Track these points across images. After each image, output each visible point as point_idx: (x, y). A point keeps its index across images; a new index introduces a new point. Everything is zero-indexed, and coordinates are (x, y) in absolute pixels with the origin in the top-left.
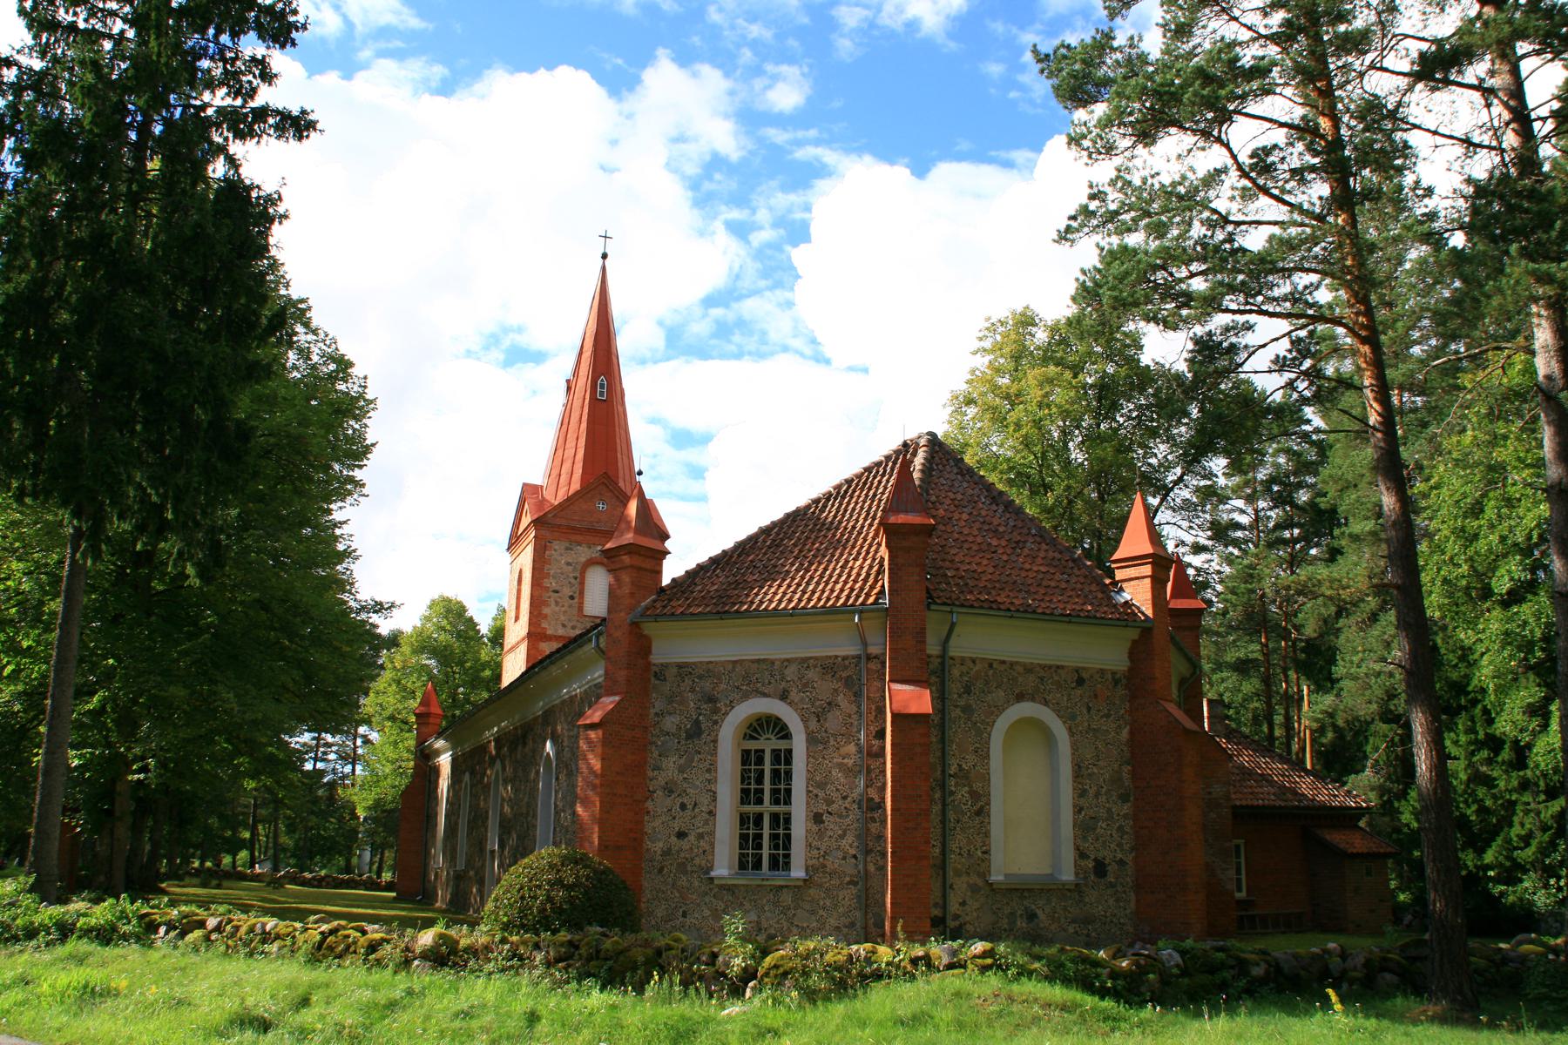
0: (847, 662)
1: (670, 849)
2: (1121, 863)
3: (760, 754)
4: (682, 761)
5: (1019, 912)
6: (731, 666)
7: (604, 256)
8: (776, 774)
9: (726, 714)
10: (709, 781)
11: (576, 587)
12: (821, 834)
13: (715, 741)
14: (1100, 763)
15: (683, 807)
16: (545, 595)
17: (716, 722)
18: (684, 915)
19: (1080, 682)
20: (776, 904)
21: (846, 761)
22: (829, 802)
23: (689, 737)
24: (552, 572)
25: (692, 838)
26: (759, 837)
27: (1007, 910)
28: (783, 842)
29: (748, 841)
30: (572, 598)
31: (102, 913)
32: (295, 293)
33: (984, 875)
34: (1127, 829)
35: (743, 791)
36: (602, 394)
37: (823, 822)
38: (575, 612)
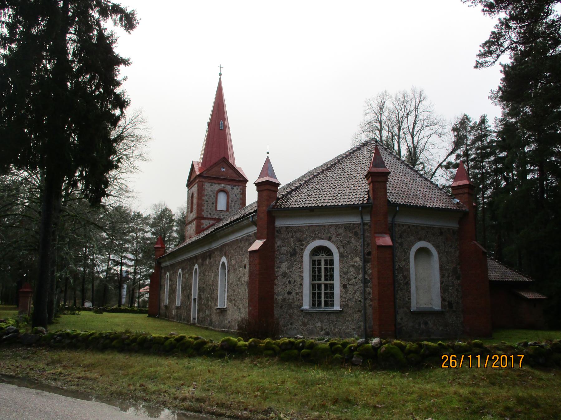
0: (355, 226)
1: (285, 299)
2: (458, 303)
3: (319, 262)
5: (422, 322)
7: (220, 75)
8: (326, 270)
9: (306, 246)
10: (300, 272)
11: (214, 200)
12: (346, 292)
13: (302, 257)
15: (290, 282)
17: (302, 249)
18: (291, 324)
19: (441, 233)
21: (355, 264)
25: (294, 294)
28: (330, 295)
33: (409, 308)
34: (460, 290)
35: (313, 276)
36: (221, 127)
37: (347, 288)
38: (214, 208)
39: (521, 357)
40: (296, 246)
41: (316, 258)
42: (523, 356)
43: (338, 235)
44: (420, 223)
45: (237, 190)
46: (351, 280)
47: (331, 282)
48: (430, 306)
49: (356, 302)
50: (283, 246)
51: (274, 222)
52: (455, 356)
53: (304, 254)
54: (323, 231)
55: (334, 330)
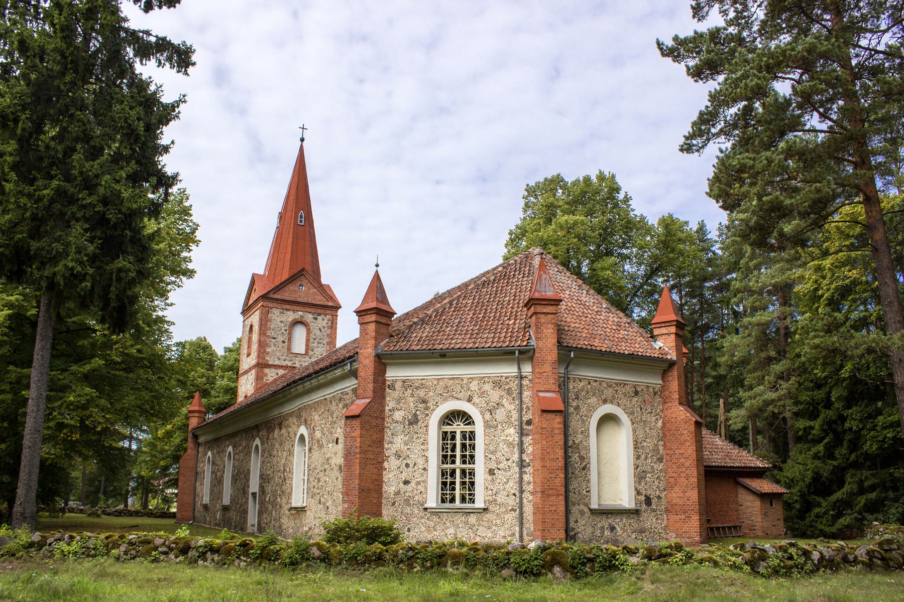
0: (508, 380)
1: (399, 491)
4: (406, 438)
6: (436, 382)
7: (302, 140)
11: (286, 337)
13: (427, 426)
15: (407, 465)
16: (268, 340)
18: (409, 530)
19: (636, 393)
20: (466, 523)
21: (508, 438)
22: (498, 463)
23: (411, 424)
24: (272, 327)
25: (413, 484)
26: (453, 483)
27: (599, 525)
29: (446, 485)
30: (284, 342)
31: (528, 509)
36: (301, 221)
37: (494, 474)
38: (285, 350)
40: (417, 410)
41: (448, 429)
45: (323, 321)
54: (459, 386)
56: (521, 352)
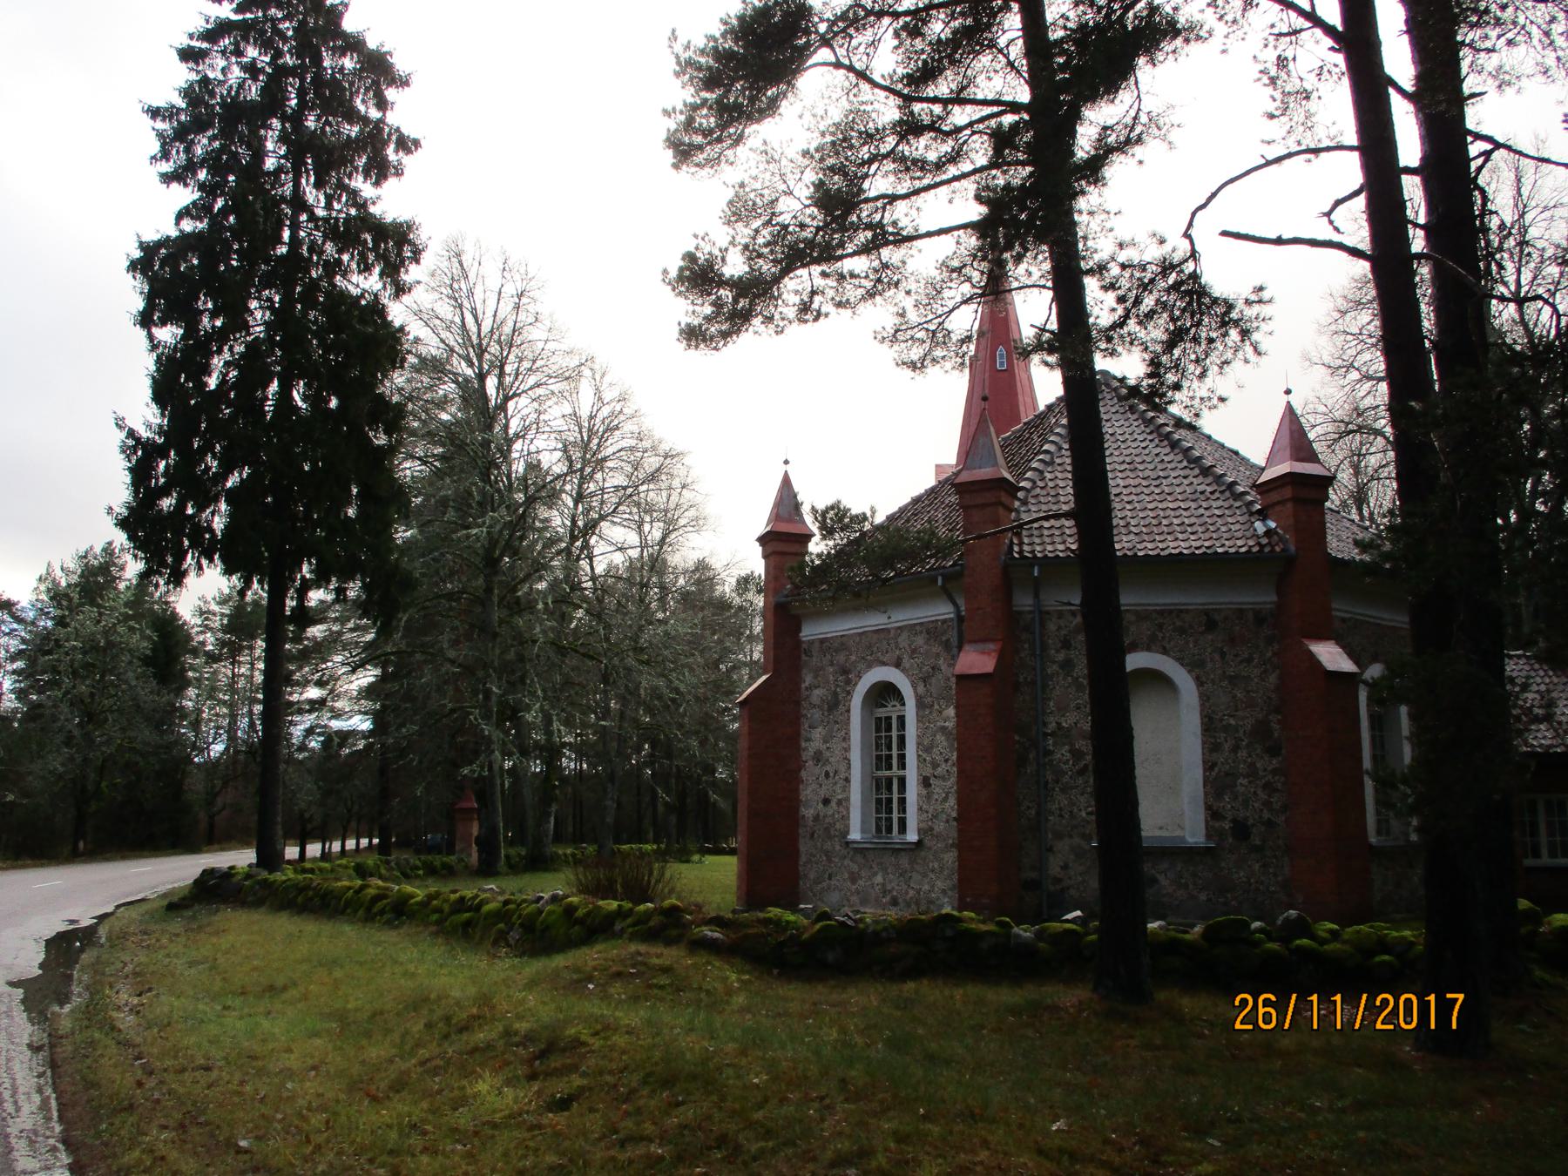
2: (1270, 824)
9: (856, 684)
13: (848, 711)
14: (1240, 713)
15: (827, 775)
18: (830, 878)
19: (1211, 625)
25: (833, 804)
32: (1107, 175)
39: (1457, 1000)
41: (881, 713)
42: (1461, 997)
43: (914, 651)
44: (1132, 602)
46: (938, 766)
47: (901, 773)
48: (1178, 833)
49: (947, 821)
50: (816, 688)
51: (799, 630)
52: (1273, 998)
53: (853, 704)
54: (885, 642)
55: (907, 893)
56: (945, 578)
